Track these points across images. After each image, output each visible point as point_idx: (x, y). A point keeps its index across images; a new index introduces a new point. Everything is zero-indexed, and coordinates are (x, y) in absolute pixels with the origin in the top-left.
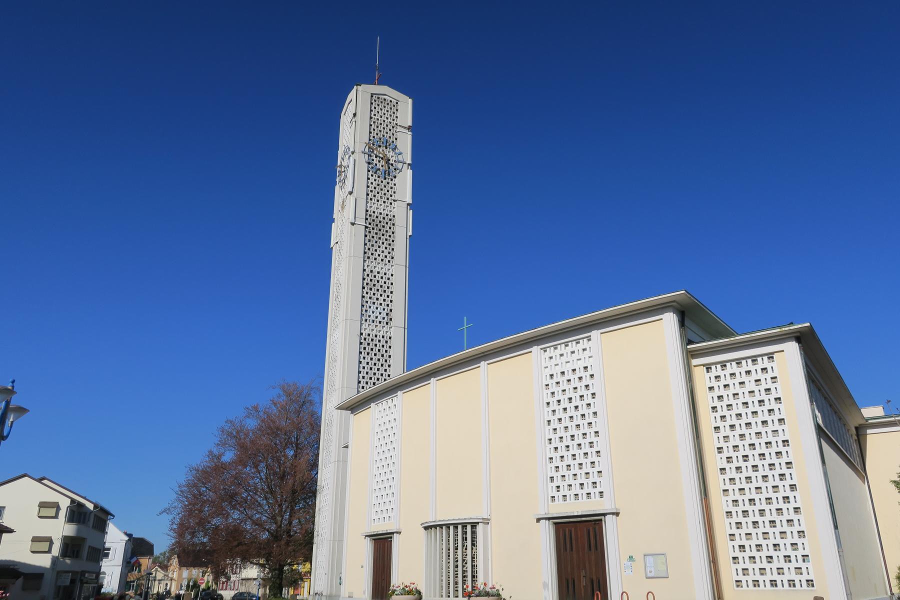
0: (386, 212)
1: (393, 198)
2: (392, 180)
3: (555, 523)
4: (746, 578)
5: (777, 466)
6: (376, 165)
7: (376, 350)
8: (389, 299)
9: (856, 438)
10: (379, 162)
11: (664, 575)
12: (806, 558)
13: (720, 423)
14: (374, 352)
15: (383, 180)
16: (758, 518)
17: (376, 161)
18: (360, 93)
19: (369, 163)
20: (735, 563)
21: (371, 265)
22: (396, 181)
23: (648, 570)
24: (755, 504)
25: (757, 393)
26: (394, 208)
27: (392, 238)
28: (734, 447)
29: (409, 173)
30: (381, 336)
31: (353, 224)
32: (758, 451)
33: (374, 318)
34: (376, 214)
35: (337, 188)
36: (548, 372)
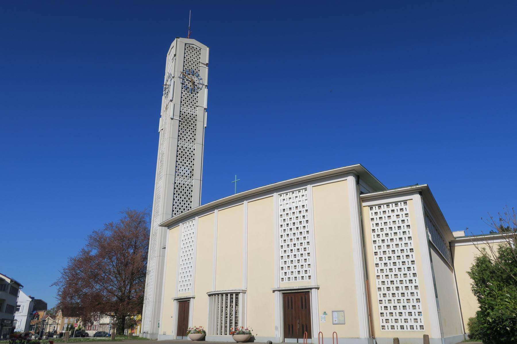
0: (192, 113)
1: (196, 105)
2: (196, 94)
3: (283, 293)
4: (387, 324)
5: (407, 263)
6: (187, 85)
7: (183, 192)
8: (192, 163)
9: (449, 248)
10: (189, 83)
11: (344, 323)
12: (420, 313)
13: (376, 239)
14: (182, 194)
15: (190, 94)
16: (395, 291)
17: (187, 82)
18: (178, 43)
19: (183, 84)
20: (382, 316)
21: (182, 143)
22: (198, 95)
23: (334, 320)
24: (394, 284)
25: (397, 222)
26: (196, 110)
27: (195, 128)
28: (383, 252)
29: (206, 91)
30: (187, 185)
31: (172, 119)
32: (397, 254)
33: (183, 174)
34: (186, 114)
35: (163, 97)
36: (282, 208)
